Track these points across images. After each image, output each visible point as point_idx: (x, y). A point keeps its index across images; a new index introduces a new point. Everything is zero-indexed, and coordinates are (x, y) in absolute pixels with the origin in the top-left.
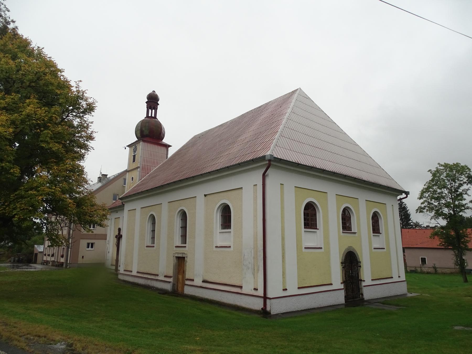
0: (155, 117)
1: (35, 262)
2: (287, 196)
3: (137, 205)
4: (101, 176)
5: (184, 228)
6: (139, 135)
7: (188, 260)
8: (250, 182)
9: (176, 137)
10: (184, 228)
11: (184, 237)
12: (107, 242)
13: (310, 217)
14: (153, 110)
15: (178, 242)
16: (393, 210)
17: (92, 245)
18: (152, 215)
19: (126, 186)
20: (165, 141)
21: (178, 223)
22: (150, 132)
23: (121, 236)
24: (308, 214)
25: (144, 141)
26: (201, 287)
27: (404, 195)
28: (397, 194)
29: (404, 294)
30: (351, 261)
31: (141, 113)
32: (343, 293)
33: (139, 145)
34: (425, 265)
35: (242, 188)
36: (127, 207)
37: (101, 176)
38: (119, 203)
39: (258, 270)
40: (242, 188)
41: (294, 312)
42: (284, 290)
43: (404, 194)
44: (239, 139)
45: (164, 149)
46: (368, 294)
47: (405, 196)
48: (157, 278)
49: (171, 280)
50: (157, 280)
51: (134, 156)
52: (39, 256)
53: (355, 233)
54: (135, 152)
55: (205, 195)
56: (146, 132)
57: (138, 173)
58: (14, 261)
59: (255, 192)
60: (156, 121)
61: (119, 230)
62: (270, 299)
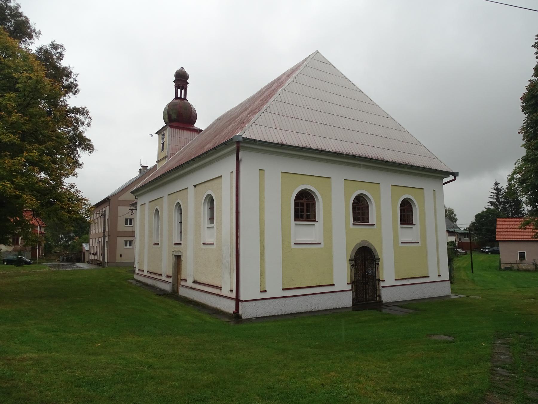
0: (185, 98)
1: (83, 262)
2: (268, 188)
6: (167, 120)
7: (183, 258)
8: (225, 168)
13: (305, 207)
14: (183, 91)
16: (435, 197)
17: (130, 242)
22: (179, 116)
24: (302, 205)
25: (171, 127)
26: (192, 288)
28: (443, 176)
29: (446, 296)
30: (364, 260)
31: (168, 94)
32: (350, 295)
34: (524, 262)
35: (221, 176)
39: (233, 270)
40: (221, 176)
41: (275, 316)
42: (261, 292)
43: (451, 176)
47: (453, 178)
49: (170, 280)
51: (163, 144)
52: (87, 254)
53: (373, 225)
55: (195, 186)
56: (174, 116)
58: (63, 260)
60: (185, 103)
62: (242, 301)
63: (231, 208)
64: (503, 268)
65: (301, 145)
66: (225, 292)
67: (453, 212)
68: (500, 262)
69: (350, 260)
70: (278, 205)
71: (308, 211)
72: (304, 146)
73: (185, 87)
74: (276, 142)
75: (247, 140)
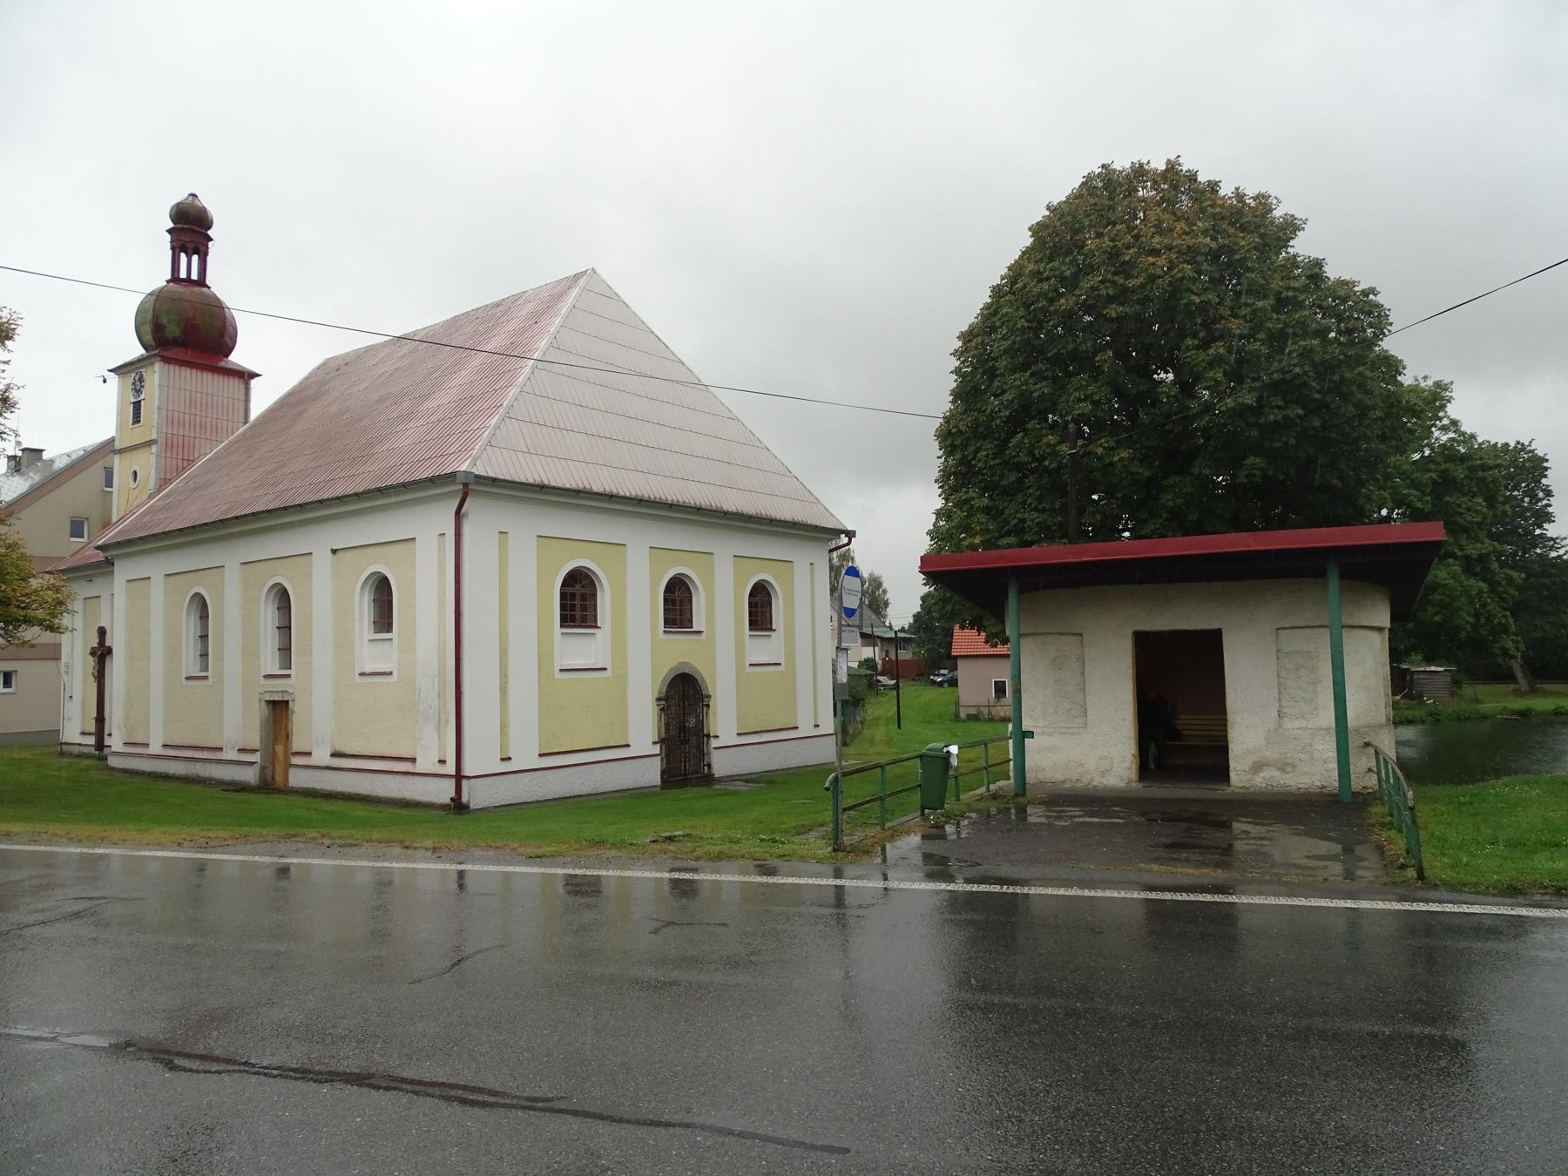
0: (202, 282)
2: (515, 564)
3: (156, 568)
4: (20, 454)
5: (285, 628)
6: (149, 338)
7: (297, 707)
8: (429, 526)
9: (275, 354)
10: (285, 628)
11: (285, 650)
12: (63, 669)
13: (578, 601)
14: (195, 258)
15: (271, 664)
18: (197, 595)
19: (115, 489)
20: (238, 357)
21: (268, 616)
22: (188, 333)
23: (110, 651)
24: (573, 596)
25: (166, 360)
26: (328, 768)
27: (845, 540)
30: (684, 698)
31: (152, 267)
33: (149, 370)
34: (1003, 701)
36: (124, 571)
37: (20, 454)
38: (101, 556)
39: (447, 722)
44: (425, 406)
45: (234, 384)
46: (721, 764)
48: (218, 756)
49: (256, 757)
50: (219, 761)
54: (138, 392)
55: (334, 551)
56: (173, 331)
57: (153, 459)
59: (441, 551)
60: (203, 295)
61: (102, 632)
63: (442, 605)
64: (963, 716)
65: (574, 486)
66: (426, 763)
67: (880, 585)
68: (957, 703)
69: (658, 699)
70: (536, 599)
71: (584, 608)
72: (581, 487)
73: (202, 249)
74: (531, 481)
75: (481, 480)
